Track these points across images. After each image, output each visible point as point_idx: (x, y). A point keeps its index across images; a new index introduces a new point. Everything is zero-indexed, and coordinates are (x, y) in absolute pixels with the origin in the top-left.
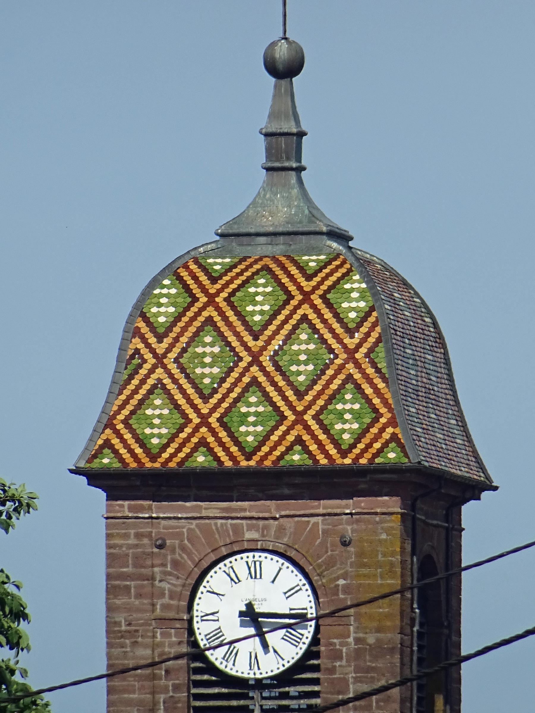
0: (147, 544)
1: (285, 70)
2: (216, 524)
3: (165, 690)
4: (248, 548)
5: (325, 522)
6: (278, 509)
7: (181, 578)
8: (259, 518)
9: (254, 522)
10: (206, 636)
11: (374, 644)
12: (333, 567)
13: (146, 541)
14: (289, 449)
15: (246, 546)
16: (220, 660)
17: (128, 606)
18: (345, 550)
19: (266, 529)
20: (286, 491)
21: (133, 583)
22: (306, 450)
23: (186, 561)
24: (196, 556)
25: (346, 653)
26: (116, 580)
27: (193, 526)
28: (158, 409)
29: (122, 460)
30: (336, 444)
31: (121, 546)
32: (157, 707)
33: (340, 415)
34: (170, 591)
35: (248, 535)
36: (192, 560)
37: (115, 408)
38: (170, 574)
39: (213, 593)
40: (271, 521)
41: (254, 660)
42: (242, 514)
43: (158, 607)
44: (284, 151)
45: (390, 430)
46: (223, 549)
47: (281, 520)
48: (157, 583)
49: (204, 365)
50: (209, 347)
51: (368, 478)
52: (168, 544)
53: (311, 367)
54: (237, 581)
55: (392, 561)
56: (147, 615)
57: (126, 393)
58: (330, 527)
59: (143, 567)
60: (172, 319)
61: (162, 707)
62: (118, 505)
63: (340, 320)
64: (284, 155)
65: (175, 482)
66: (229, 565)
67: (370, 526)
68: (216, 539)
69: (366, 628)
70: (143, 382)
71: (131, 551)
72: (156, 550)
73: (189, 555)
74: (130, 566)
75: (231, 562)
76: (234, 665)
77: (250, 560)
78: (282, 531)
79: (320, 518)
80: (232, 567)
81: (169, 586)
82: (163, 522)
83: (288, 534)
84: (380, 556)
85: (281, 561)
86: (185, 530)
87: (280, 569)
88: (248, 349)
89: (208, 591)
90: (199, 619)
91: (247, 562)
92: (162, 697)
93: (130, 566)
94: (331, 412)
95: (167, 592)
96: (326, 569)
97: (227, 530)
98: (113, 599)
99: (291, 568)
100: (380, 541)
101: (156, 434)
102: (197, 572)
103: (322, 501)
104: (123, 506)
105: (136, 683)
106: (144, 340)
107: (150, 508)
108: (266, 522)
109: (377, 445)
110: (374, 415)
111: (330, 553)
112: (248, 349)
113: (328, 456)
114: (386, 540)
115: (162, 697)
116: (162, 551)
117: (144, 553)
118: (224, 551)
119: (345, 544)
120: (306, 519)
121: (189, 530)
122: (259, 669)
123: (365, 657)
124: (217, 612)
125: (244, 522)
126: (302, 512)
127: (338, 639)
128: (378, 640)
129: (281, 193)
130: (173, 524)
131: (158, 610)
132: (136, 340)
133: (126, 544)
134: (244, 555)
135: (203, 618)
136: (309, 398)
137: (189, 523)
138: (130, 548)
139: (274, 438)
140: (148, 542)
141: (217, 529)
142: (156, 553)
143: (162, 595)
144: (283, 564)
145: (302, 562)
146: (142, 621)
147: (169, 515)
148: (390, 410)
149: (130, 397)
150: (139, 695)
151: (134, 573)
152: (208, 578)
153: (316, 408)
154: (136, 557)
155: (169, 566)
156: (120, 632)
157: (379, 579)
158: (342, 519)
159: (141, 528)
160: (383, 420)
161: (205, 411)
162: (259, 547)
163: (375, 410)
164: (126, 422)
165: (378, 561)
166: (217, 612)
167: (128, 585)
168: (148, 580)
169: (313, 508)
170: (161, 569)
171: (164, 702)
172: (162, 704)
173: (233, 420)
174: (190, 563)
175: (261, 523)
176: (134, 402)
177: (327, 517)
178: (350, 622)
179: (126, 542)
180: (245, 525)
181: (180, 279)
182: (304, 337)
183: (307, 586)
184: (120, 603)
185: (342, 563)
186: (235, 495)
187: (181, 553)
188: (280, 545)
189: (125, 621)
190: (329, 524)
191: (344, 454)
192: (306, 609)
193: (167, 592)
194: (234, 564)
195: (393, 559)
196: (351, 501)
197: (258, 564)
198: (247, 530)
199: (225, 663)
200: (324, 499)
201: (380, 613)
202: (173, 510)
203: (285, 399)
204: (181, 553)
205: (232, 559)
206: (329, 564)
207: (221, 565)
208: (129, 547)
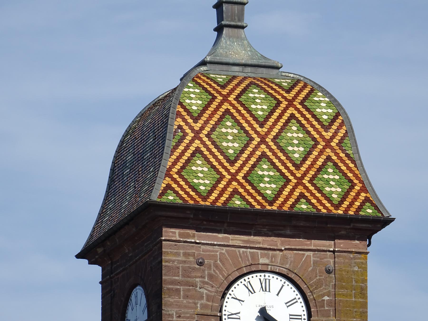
0: (192, 261)
2: (239, 251)
5: (315, 255)
6: (283, 244)
7: (215, 287)
8: (270, 249)
12: (321, 287)
13: (191, 259)
14: (297, 201)
15: (260, 268)
17: (179, 304)
18: (329, 276)
20: (288, 232)
21: (181, 287)
22: (309, 202)
23: (218, 275)
28: (199, 166)
29: (181, 198)
30: (329, 200)
31: (174, 261)
33: (327, 182)
34: (207, 296)
35: (262, 261)
36: (223, 276)
37: (170, 164)
38: (207, 283)
39: (236, 299)
43: (199, 305)
47: (285, 252)
48: (198, 288)
49: (228, 141)
50: (229, 129)
51: (352, 225)
52: (206, 263)
53: (302, 149)
54: (253, 292)
55: (362, 286)
56: (191, 311)
58: (319, 259)
59: (189, 277)
60: (202, 109)
62: (172, 232)
63: (317, 120)
64: (236, 18)
65: (217, 217)
66: (247, 280)
67: (347, 261)
68: (239, 261)
71: (181, 265)
72: (197, 266)
73: (221, 271)
77: (262, 278)
78: (285, 260)
79: (311, 253)
81: (206, 291)
82: (203, 247)
84: (354, 282)
86: (218, 253)
87: (283, 286)
88: (257, 132)
89: (232, 298)
90: (226, 317)
93: (180, 276)
94: (321, 179)
95: (204, 295)
96: (316, 288)
97: (247, 256)
98: (168, 298)
100: (354, 271)
101: (203, 183)
102: (226, 284)
103: (313, 241)
106: (184, 120)
107: (194, 236)
108: (275, 252)
109: (357, 204)
110: (350, 184)
111: (318, 278)
112: (257, 132)
114: (357, 271)
116: (202, 267)
117: (190, 268)
118: (245, 271)
119: (328, 272)
120: (302, 252)
121: (221, 253)
124: (239, 313)
125: (259, 251)
126: (300, 247)
129: (236, 42)
131: (199, 308)
133: (178, 260)
134: (258, 274)
136: (303, 169)
138: (180, 263)
139: (286, 193)
142: (197, 269)
143: (202, 298)
144: (285, 283)
147: (208, 242)
148: (361, 182)
152: (233, 288)
153: (309, 176)
154: (184, 270)
157: (354, 298)
158: (327, 255)
159: (188, 250)
160: (357, 188)
161: (233, 171)
162: (269, 270)
163: (350, 181)
164: (179, 173)
165: (353, 285)
166: (239, 313)
169: (306, 245)
170: (201, 279)
173: (253, 178)
174: (221, 276)
175: (271, 252)
176: (182, 161)
179: (177, 259)
180: (259, 253)
181: (197, 83)
182: (294, 128)
183: (301, 300)
185: (326, 285)
186: (252, 232)
187: (215, 269)
188: (284, 269)
189: (176, 313)
190: (318, 257)
191: (337, 207)
192: (301, 316)
193: (204, 295)
194: (251, 279)
197: (267, 281)
198: (261, 258)
202: (209, 238)
203: (287, 168)
205: (250, 276)
206: (317, 285)
207: (242, 280)
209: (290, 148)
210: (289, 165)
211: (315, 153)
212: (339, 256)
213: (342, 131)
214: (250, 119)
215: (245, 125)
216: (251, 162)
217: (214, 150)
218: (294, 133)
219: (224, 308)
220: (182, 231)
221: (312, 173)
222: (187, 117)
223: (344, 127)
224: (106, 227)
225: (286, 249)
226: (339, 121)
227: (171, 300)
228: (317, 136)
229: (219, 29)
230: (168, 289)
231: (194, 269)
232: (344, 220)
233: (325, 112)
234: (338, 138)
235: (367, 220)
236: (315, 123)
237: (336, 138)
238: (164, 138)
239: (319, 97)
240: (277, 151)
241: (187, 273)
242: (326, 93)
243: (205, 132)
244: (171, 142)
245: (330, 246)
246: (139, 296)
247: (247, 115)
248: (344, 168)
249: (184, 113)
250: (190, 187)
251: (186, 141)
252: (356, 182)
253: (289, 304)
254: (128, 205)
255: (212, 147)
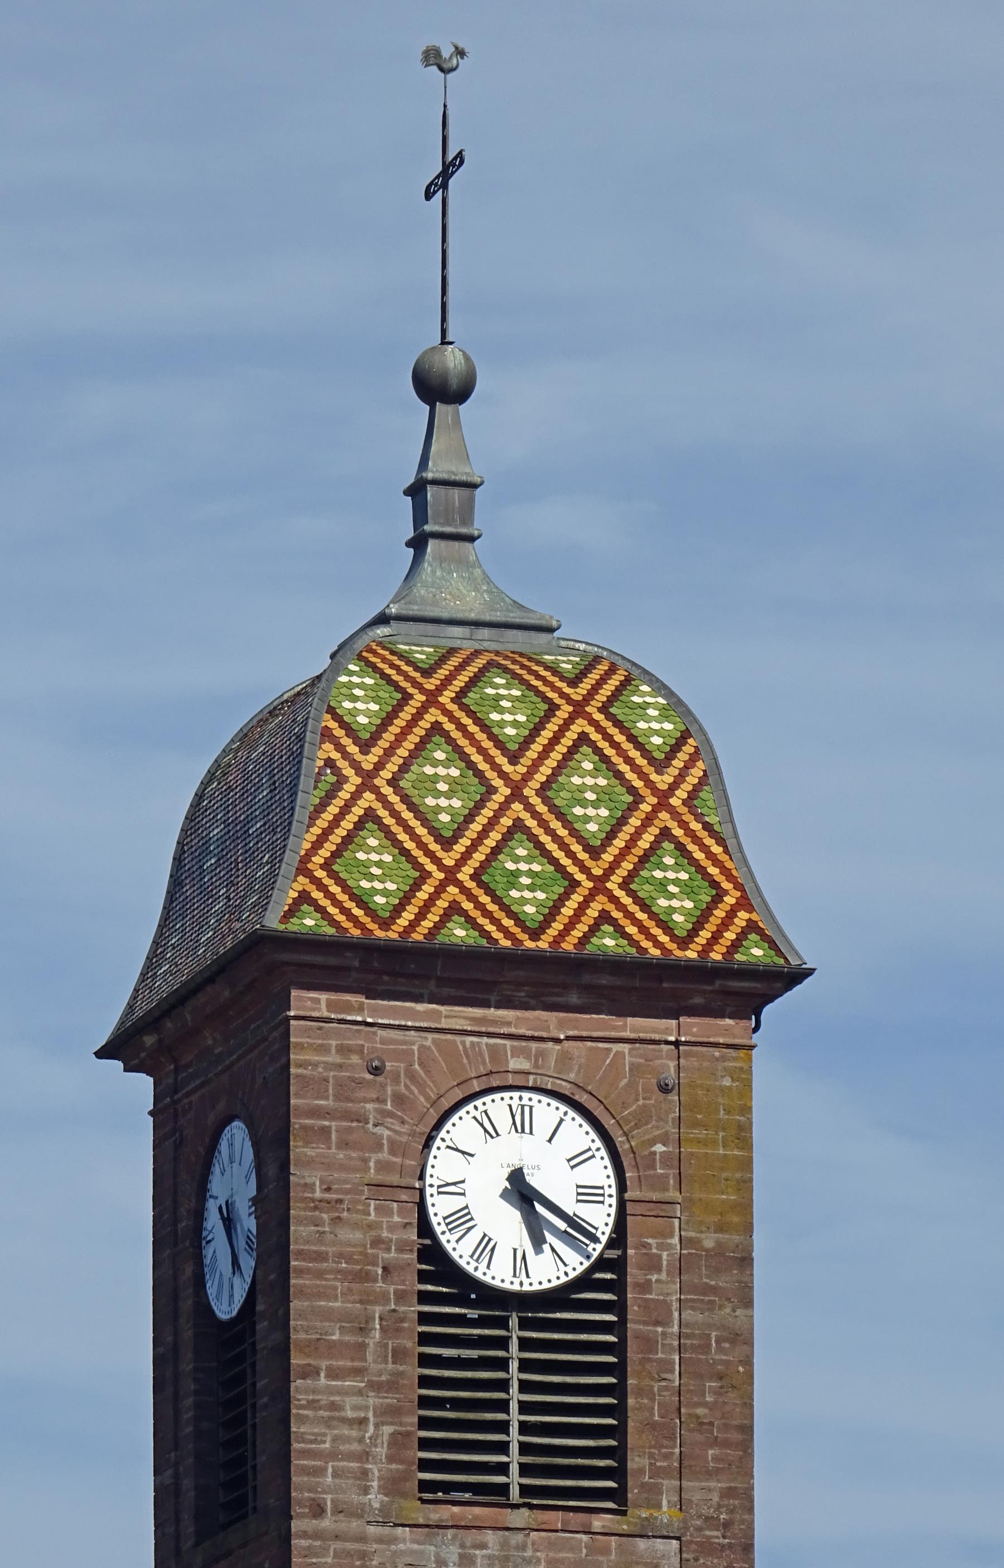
0: (358, 1064)
1: (440, 389)
2: (463, 1043)
3: (383, 1298)
4: (515, 1084)
5: (635, 1052)
6: (561, 1025)
7: (408, 1123)
9: (524, 1044)
10: (445, 1218)
11: (713, 1249)
12: (647, 1123)
14: (594, 929)
15: (510, 1080)
16: (466, 1258)
19: (541, 1055)
20: (574, 999)
21: (333, 1123)
22: (620, 932)
23: (415, 1096)
24: (432, 1090)
25: (668, 1261)
26: (308, 1117)
27: (428, 1043)
29: (333, 922)
30: (667, 928)
31: (315, 1065)
32: (370, 1325)
35: (514, 1064)
36: (427, 1098)
37: (307, 845)
38: (391, 1115)
40: (550, 1044)
41: (520, 1263)
42: (504, 1030)
43: (372, 1164)
44: (436, 511)
45: (743, 915)
46: (475, 1082)
47: (567, 1044)
48: (370, 1126)
49: (438, 794)
50: (440, 767)
52: (387, 1068)
53: (604, 812)
57: (322, 823)
59: (349, 1100)
61: (378, 1327)
63: (639, 746)
66: (481, 1108)
67: (705, 1064)
68: (463, 1064)
69: (701, 1222)
70: (346, 809)
71: (332, 1074)
73: (422, 1087)
74: (331, 1097)
75: (484, 1104)
76: (488, 1267)
77: (515, 1103)
78: (567, 1061)
79: (625, 1047)
80: (485, 1112)
82: (381, 1033)
83: (576, 1068)
84: (722, 1112)
85: (563, 1108)
86: (415, 1048)
87: (562, 1120)
88: (502, 775)
90: (434, 1191)
91: (510, 1106)
92: (378, 1310)
93: (331, 1097)
95: (385, 1142)
96: (637, 1126)
97: (481, 1054)
99: (579, 1120)
100: (722, 1089)
103: (629, 1019)
104: (317, 1001)
105: (339, 1284)
106: (340, 748)
107: (360, 1009)
109: (730, 935)
110: (714, 892)
111: (641, 1102)
112: (502, 775)
113: (657, 944)
114: (730, 1088)
115: (378, 1310)
116: (379, 1079)
117: (352, 1079)
118: (476, 1086)
119: (665, 1089)
121: (422, 1047)
122: (528, 1276)
123: (700, 1269)
124: (463, 1182)
125: (508, 1043)
127: (654, 1237)
128: (719, 1244)
129: (457, 572)
130: (396, 1037)
131: (372, 1171)
132: (328, 746)
133: (324, 1062)
134: (506, 1095)
135: (440, 1190)
137: (421, 1037)
140: (360, 1061)
141: (465, 1050)
142: (369, 1082)
143: (379, 1147)
144: (566, 1114)
145: (598, 1112)
146: (349, 1186)
147: (392, 1022)
148: (738, 886)
149: (326, 833)
150: (343, 1302)
151: (336, 1109)
152: (448, 1126)
154: (340, 1084)
155: (389, 1103)
156: (313, 1200)
158: (661, 1051)
159: (349, 1039)
160: (730, 900)
163: (714, 884)
165: (720, 1120)
167: (327, 1127)
168: (358, 1121)
169: (615, 1028)
170: (376, 1106)
171: (381, 1319)
172: (377, 1321)
173: (494, 877)
174: (422, 1099)
175: (534, 1045)
177: (637, 1045)
178: (675, 1212)
180: (508, 1047)
182: (588, 766)
183: (603, 1152)
184: (314, 1154)
185: (659, 1119)
186: (493, 999)
187: (409, 1083)
188: (564, 1083)
189: (322, 1182)
190: (640, 1057)
191: (684, 943)
193: (385, 1142)
194: (490, 1106)
195: (742, 1118)
196: (674, 1022)
197: (527, 1109)
198: (512, 1057)
199: (473, 1264)
200: (634, 1016)
201: (723, 1201)
204: (409, 1083)
205: (487, 1099)
207: (470, 1107)
208: (329, 1066)
209: (578, 811)
210: (577, 848)
211: (635, 822)
212: (688, 1055)
213: (696, 773)
214: (487, 744)
215: (476, 758)
216: (490, 842)
217: (407, 815)
218: (586, 777)
219: (429, 1171)
220: (334, 996)
221: (627, 866)
222: (346, 741)
223: (700, 764)
224: (164, 986)
225: (568, 1038)
226: (688, 749)
227: (310, 1152)
228: (638, 784)
229: (418, 543)
230: (304, 1128)
231: (361, 1082)
232: (701, 972)
233: (656, 728)
234: (687, 787)
235: (751, 972)
236: (634, 754)
237: (680, 790)
238: (293, 789)
239: (643, 694)
240: (548, 817)
241: (345, 1090)
242: (660, 687)
243: (386, 774)
244: (308, 797)
245: (667, 1031)
246: (237, 1138)
247: (481, 736)
248: (699, 855)
249: (339, 733)
250: (353, 897)
251: (344, 795)
252: (726, 886)
253: (576, 1161)
254: (211, 940)
255: (401, 807)
